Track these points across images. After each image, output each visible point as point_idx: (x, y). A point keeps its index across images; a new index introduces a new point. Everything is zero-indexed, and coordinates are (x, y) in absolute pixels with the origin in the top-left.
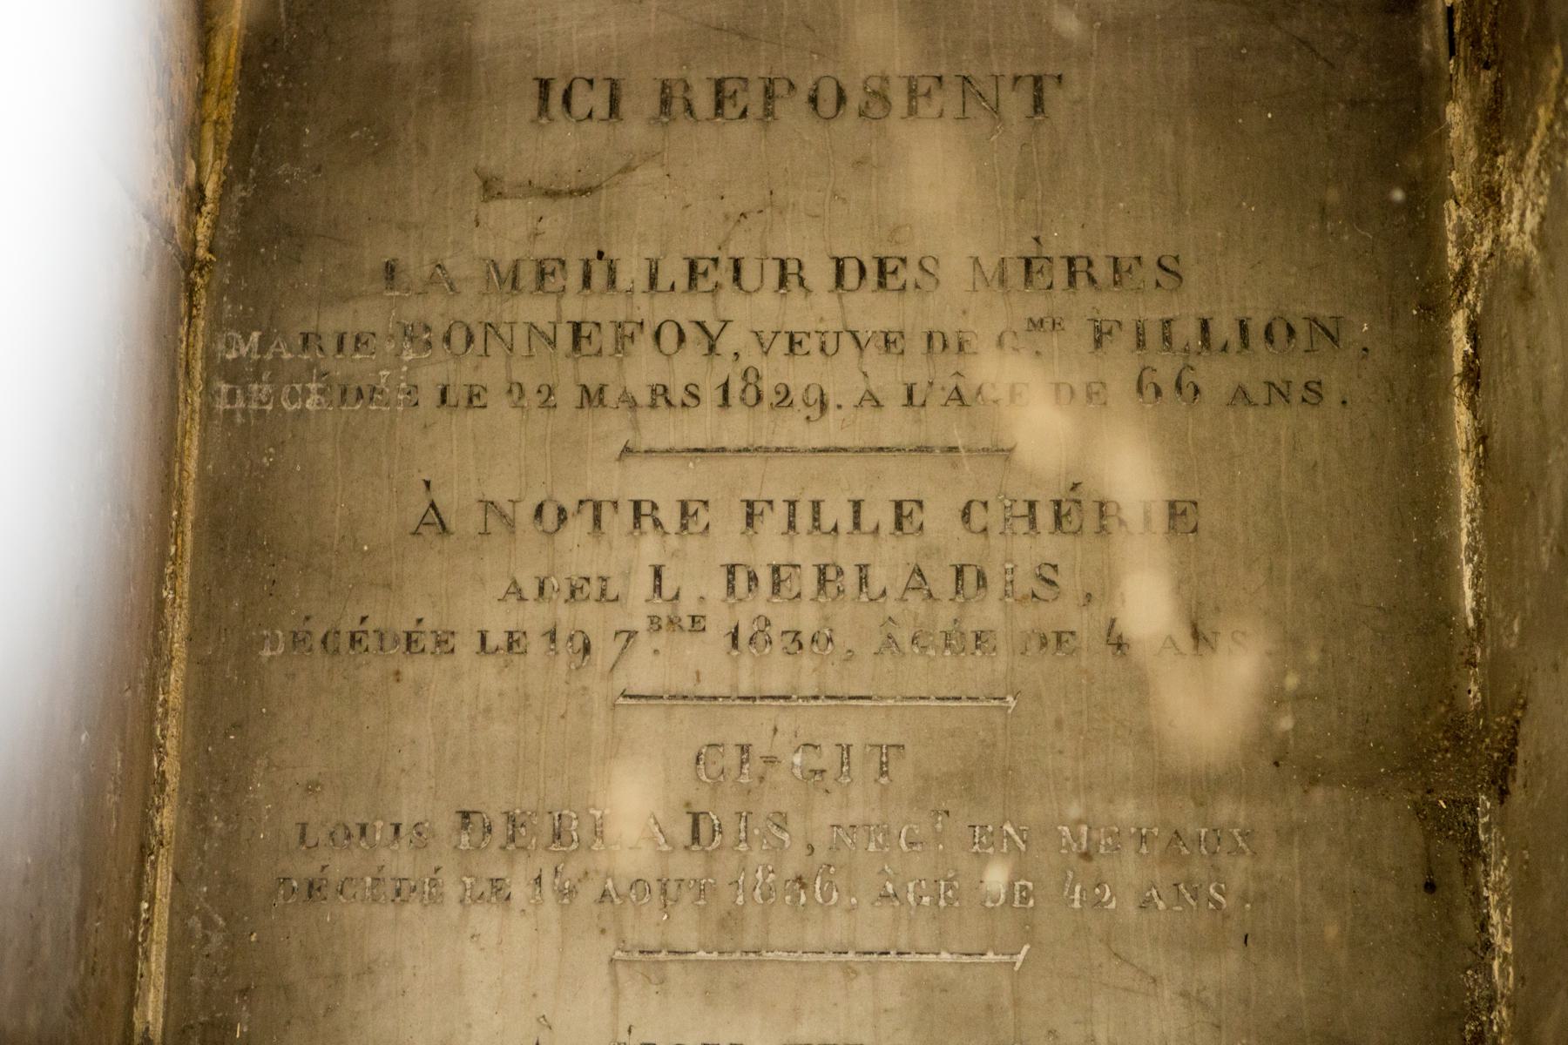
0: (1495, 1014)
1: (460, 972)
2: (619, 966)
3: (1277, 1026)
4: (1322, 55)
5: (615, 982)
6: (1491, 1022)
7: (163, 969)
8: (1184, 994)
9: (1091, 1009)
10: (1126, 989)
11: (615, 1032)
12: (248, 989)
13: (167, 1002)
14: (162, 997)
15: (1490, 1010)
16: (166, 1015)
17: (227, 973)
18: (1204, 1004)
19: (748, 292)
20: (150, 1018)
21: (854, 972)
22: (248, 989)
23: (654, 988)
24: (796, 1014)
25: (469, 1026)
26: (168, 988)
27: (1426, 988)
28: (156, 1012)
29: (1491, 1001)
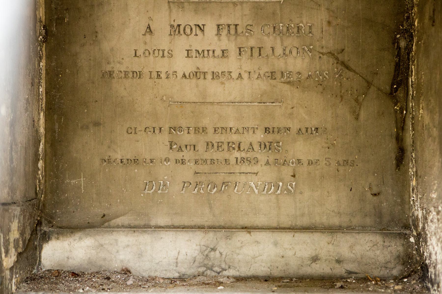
0: (413, 11)
1: (126, 4)
2: (171, 3)
3: (353, 17)
4: (295, 126)
5: (170, 7)
6: (412, 13)
7: (44, 3)
8: (328, 9)
9: (302, 14)
10: (311, 8)
11: (170, 21)
12: (68, 9)
13: (45, 12)
14: (44, 11)
15: (412, 10)
16: (45, 16)
17: (62, 4)
18: (333, 12)
19: (138, 57)
20: (41, 15)
21: (237, 5)
22: (68, 9)
23: (181, 9)
24: (220, 16)
25: (130, 20)
26: (45, 8)
27: (395, 5)
28: (42, 14)
29: (413, 7)
